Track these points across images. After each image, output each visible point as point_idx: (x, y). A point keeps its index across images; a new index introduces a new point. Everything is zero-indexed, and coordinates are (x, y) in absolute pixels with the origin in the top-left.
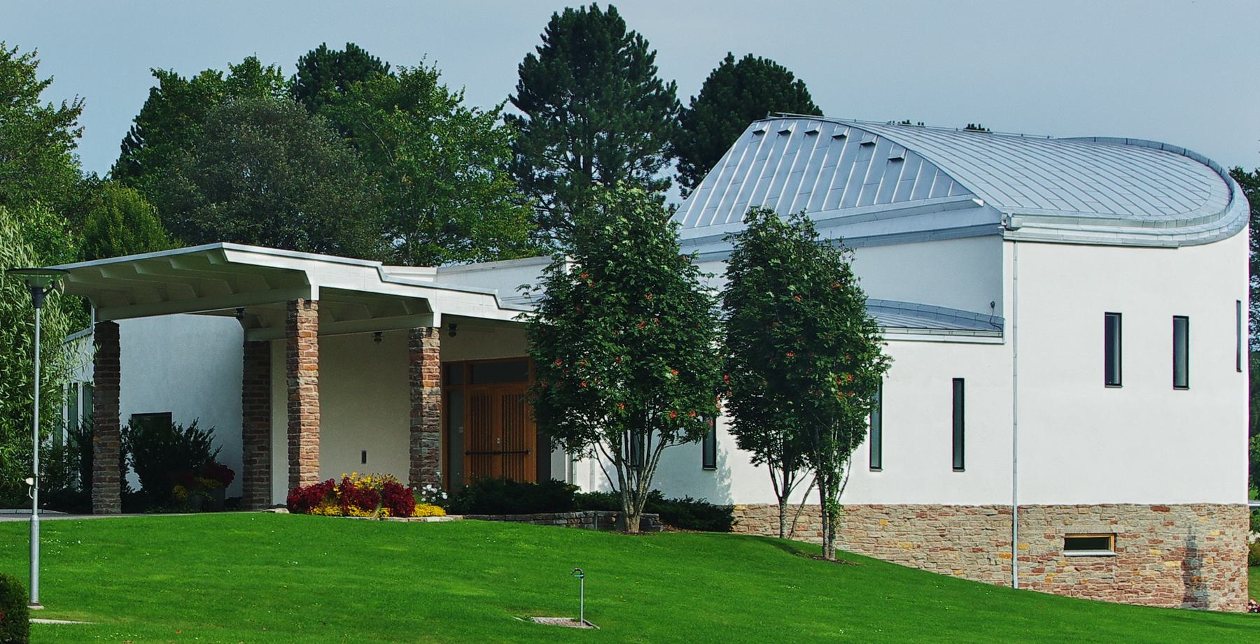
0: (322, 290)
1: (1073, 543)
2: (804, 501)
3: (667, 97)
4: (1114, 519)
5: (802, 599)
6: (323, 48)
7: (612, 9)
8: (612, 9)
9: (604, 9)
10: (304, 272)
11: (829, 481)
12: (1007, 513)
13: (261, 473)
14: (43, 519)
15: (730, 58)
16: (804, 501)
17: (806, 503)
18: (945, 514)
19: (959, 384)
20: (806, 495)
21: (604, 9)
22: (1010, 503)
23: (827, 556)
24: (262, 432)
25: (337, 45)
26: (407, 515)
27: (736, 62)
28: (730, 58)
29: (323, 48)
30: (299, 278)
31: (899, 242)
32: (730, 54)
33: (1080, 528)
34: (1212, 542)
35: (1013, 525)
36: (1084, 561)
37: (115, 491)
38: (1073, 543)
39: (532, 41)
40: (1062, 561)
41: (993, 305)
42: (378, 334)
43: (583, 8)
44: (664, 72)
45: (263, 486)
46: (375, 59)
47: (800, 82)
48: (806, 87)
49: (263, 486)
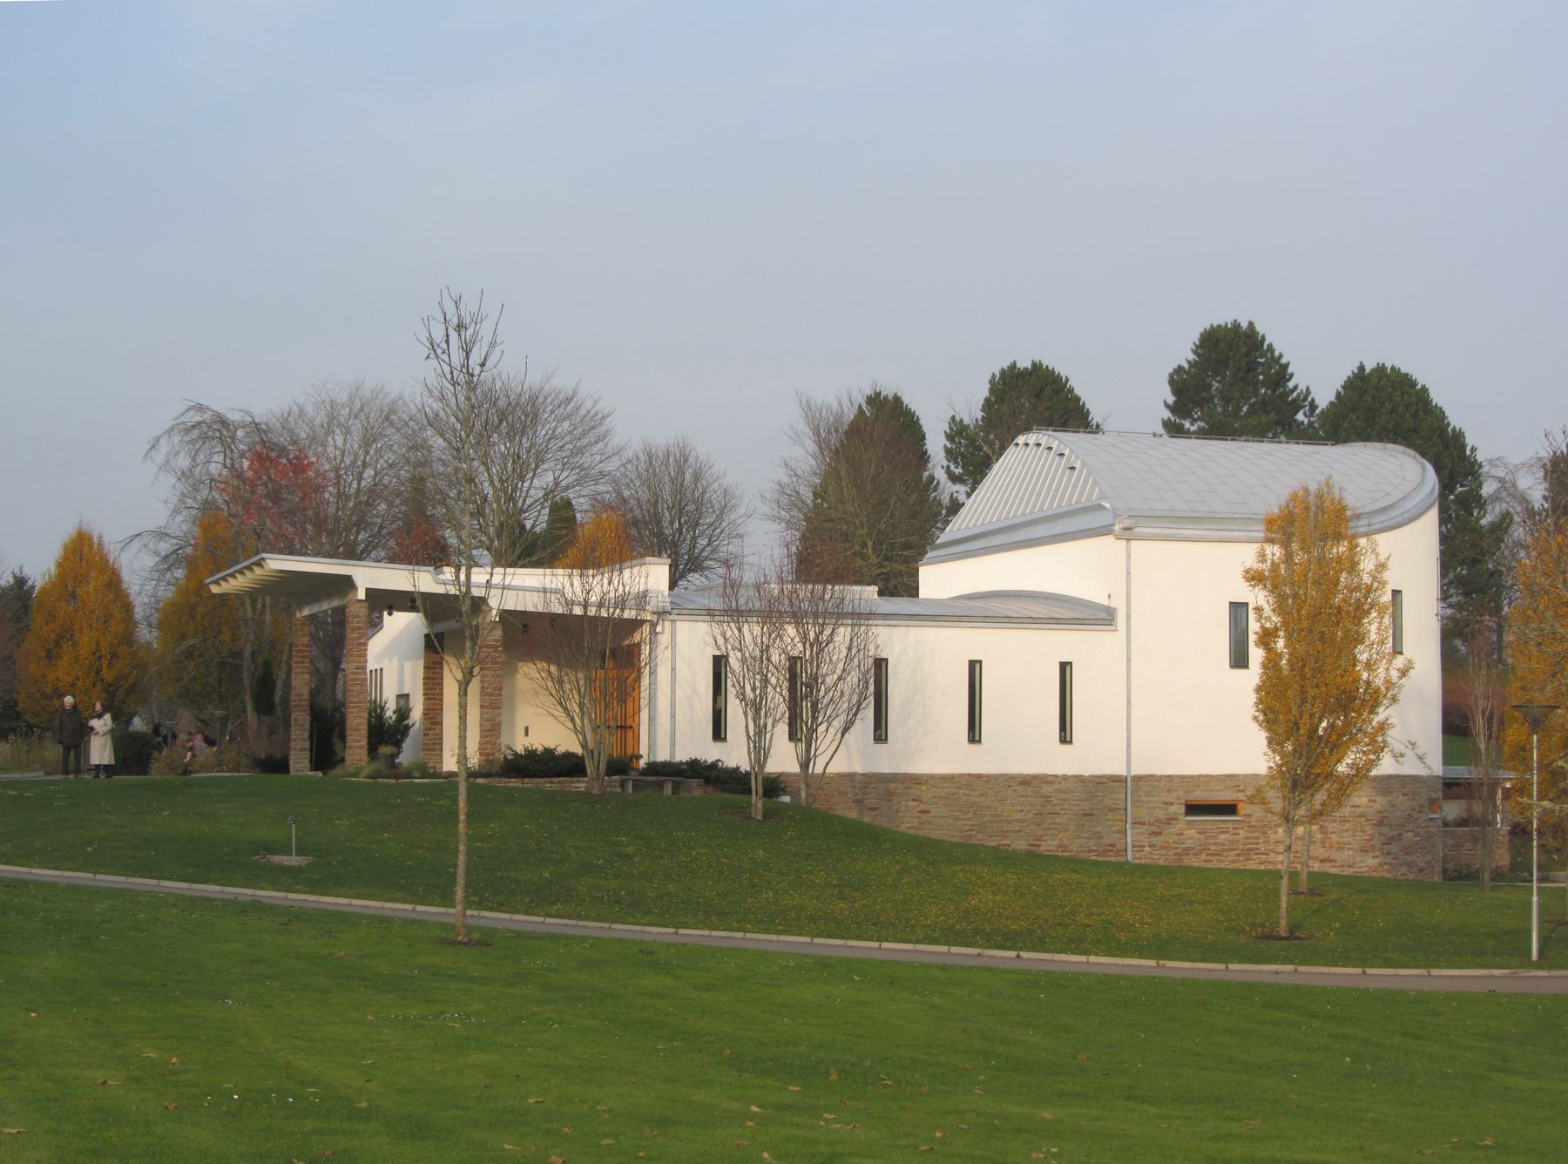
1: (1193, 809)
4: (1241, 788)
7: (1251, 324)
8: (1251, 324)
9: (1244, 325)
10: (350, 576)
12: (1121, 781)
13: (434, 744)
15: (1361, 368)
17: (827, 771)
18: (1052, 783)
19: (1065, 668)
21: (1244, 325)
22: (1123, 772)
24: (435, 710)
25: (1024, 363)
26: (146, 773)
27: (1367, 371)
28: (1361, 368)
29: (1014, 366)
30: (347, 583)
33: (1200, 796)
35: (1126, 793)
37: (304, 758)
39: (1182, 353)
41: (1109, 596)
44: (1300, 379)
47: (1423, 387)
48: (916, 413)
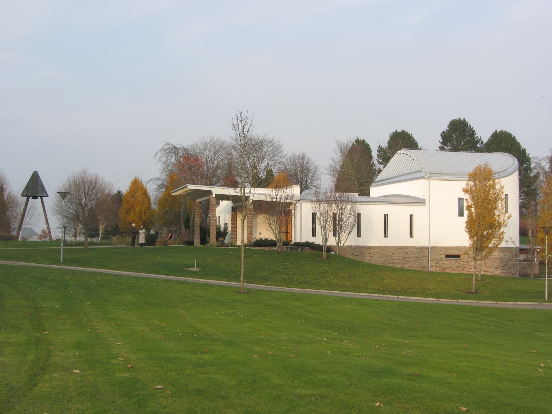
1: (448, 256)
2: (344, 244)
7: (464, 119)
8: (464, 119)
9: (462, 119)
13: (234, 237)
15: (496, 131)
16: (344, 244)
18: (408, 248)
19: (411, 216)
20: (344, 243)
21: (462, 119)
22: (427, 246)
23: (324, 257)
25: (399, 130)
27: (498, 132)
29: (397, 131)
33: (450, 252)
38: (448, 256)
39: (445, 127)
40: (444, 261)
42: (260, 204)
44: (478, 134)
45: (235, 240)
49: (235, 240)
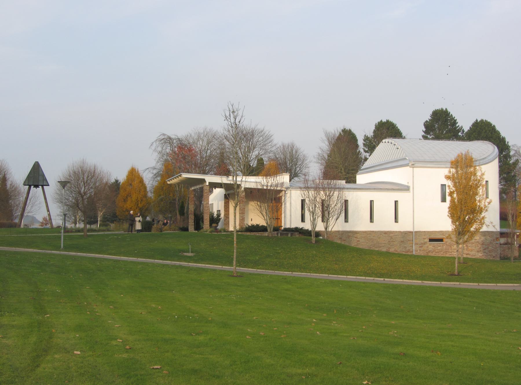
0: (209, 183)
1: (431, 240)
3: (461, 129)
5: (288, 253)
6: (381, 121)
7: (446, 109)
8: (446, 109)
9: (444, 109)
11: (90, 226)
14: (64, 234)
15: (477, 120)
18: (393, 233)
19: (396, 202)
21: (444, 109)
25: (384, 120)
27: (478, 121)
31: (398, 167)
32: (477, 119)
33: (433, 237)
34: (476, 240)
36: (435, 245)
38: (431, 240)
39: (427, 117)
43: (439, 109)
46: (455, 119)
